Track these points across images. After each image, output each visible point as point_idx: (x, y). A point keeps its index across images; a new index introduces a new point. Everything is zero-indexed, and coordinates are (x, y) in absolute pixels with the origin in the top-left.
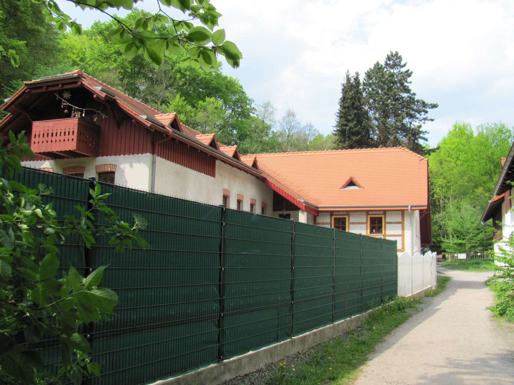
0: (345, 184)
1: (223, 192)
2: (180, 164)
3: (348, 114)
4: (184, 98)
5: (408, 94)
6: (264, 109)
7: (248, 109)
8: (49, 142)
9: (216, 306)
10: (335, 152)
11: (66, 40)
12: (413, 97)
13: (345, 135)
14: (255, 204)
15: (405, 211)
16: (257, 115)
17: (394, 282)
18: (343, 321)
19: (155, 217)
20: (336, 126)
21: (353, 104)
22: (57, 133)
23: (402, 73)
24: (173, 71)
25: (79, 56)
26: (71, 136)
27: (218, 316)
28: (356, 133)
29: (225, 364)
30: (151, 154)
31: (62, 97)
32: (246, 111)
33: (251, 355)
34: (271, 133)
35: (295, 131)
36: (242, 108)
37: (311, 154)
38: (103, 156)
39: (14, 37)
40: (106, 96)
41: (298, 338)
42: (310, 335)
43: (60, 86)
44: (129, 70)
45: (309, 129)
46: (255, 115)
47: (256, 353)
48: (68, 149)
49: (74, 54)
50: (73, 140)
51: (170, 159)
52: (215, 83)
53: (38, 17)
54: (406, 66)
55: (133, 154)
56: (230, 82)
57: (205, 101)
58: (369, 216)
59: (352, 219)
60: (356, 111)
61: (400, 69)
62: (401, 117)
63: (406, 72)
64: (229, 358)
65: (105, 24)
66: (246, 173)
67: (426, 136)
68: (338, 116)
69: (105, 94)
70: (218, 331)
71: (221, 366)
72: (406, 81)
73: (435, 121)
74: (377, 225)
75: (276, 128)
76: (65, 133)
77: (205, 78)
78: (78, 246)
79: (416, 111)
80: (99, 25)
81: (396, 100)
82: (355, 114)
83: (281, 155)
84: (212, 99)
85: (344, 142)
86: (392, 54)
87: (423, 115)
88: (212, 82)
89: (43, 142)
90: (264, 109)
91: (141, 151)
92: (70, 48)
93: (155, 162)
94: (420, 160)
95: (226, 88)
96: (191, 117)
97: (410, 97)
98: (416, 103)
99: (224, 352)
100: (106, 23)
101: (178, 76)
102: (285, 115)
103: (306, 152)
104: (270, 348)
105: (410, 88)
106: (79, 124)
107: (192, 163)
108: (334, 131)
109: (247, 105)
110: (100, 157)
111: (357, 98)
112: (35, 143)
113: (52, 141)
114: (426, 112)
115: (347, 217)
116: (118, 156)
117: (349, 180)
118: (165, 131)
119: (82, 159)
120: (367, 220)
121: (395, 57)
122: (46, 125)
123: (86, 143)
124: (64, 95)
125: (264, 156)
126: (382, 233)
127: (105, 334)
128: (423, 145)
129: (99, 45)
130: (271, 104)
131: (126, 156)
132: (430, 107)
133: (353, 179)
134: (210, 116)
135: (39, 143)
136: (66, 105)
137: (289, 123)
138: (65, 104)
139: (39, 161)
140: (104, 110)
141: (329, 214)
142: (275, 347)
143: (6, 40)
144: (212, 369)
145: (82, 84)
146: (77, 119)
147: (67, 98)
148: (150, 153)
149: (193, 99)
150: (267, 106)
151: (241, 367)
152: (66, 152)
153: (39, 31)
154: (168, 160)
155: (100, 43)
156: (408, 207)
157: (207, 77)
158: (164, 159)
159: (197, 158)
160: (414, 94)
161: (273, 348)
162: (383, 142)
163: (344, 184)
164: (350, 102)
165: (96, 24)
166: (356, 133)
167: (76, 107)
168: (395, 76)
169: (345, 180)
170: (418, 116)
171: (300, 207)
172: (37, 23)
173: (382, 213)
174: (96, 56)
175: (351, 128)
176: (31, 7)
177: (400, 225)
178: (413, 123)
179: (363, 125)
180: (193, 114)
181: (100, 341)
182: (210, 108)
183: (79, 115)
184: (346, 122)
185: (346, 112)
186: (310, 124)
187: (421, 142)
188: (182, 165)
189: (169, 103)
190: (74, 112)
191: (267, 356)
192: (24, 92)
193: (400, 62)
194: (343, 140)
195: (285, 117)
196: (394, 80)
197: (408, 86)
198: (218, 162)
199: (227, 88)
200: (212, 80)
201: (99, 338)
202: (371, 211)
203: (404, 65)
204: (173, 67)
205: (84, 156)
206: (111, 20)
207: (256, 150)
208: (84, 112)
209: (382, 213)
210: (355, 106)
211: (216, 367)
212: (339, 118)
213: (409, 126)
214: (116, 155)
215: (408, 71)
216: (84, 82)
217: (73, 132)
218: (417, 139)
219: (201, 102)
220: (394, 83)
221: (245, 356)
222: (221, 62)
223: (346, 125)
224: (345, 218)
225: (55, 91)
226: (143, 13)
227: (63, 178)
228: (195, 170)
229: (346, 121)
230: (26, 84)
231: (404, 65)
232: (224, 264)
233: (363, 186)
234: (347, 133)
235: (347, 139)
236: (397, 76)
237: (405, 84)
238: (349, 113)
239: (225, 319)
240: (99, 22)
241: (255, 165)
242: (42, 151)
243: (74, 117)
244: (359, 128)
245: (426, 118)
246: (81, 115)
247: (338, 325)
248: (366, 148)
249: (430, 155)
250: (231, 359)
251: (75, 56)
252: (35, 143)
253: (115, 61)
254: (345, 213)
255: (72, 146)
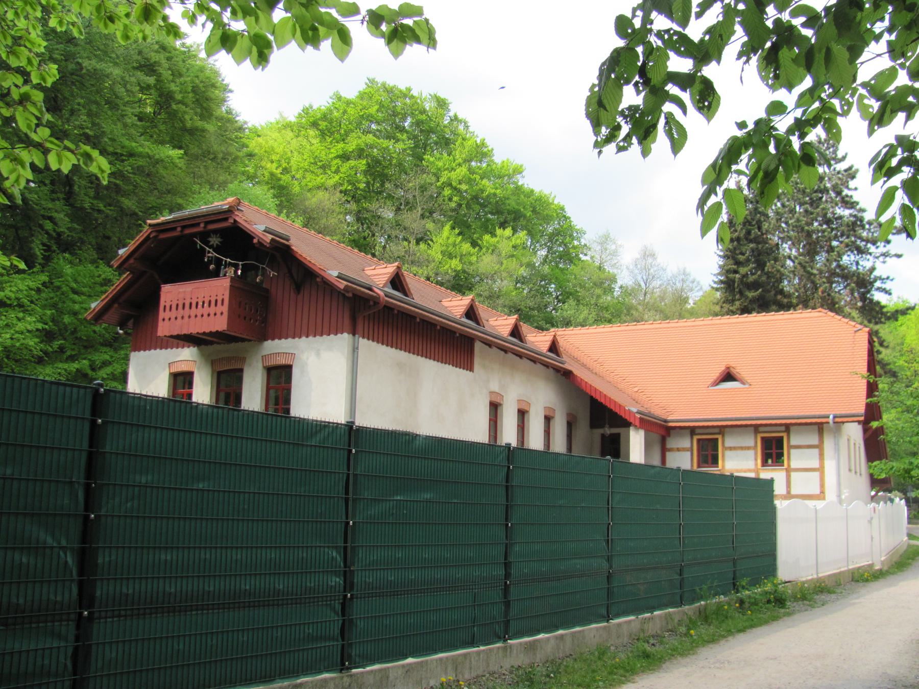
0: (718, 378)
1: (490, 396)
2: (405, 351)
3: (738, 252)
4: (457, 231)
5: (851, 211)
6: (599, 247)
7: (574, 248)
8: (205, 316)
9: (337, 581)
10: (717, 320)
11: (260, 140)
12: (859, 215)
13: (734, 289)
14: (553, 417)
15: (825, 425)
16: (592, 258)
17: (772, 555)
18: (632, 618)
19: (192, 439)
20: (719, 274)
21: (749, 232)
22: (197, 303)
23: (839, 173)
24: (439, 184)
25: (280, 166)
26: (220, 308)
27: (341, 597)
28: (755, 286)
29: (351, 676)
30: (351, 335)
31: (207, 243)
32: (571, 251)
33: (410, 664)
34: (617, 289)
35: (656, 283)
36: (565, 245)
37: (661, 326)
38: (273, 339)
39: (162, 143)
40: (272, 240)
41: (521, 644)
42: (548, 639)
43: (202, 225)
44: (362, 186)
45: (683, 280)
46: (587, 258)
47: (422, 662)
48: (214, 330)
49: (272, 162)
50: (222, 313)
51: (385, 341)
52: (512, 203)
53: (203, 108)
54: (847, 159)
55: (322, 335)
56: (540, 200)
57: (496, 236)
58: (695, 438)
59: (730, 441)
60: (752, 245)
61: (835, 166)
62: (835, 253)
63: (846, 171)
64: (363, 666)
65: (320, 110)
66: (532, 363)
67: (888, 285)
68: (720, 256)
69: (270, 237)
70: (341, 622)
71: (343, 677)
72: (847, 187)
73: (903, 257)
74: (774, 451)
75: (624, 279)
76: (210, 302)
77: (495, 195)
78: (71, 483)
79: (867, 241)
80: (310, 111)
81: (828, 222)
82: (753, 250)
83: (632, 327)
84: (508, 232)
85: (732, 302)
86: (820, 139)
87: (882, 248)
88: (507, 202)
89: (176, 318)
90: (599, 247)
91: (333, 329)
92: (265, 152)
93: (357, 348)
94: (856, 332)
95: (532, 211)
96: (471, 264)
97: (855, 216)
98: (867, 226)
99: (353, 657)
100: (323, 108)
101: (447, 192)
102: (638, 256)
103: (676, 320)
104: (454, 656)
105: (855, 199)
106: (232, 287)
107: (420, 348)
108: (715, 282)
109: (572, 240)
110: (270, 341)
111: (754, 223)
112: (164, 320)
113: (190, 317)
114: (888, 242)
115: (720, 437)
116: (297, 339)
117: (724, 371)
118: (372, 296)
119: (240, 345)
120: (756, 442)
121: (826, 145)
122: (181, 290)
123: (245, 318)
124: (210, 239)
125: (578, 332)
126: (783, 466)
127: (116, 613)
128: (883, 303)
129: (312, 145)
130: (612, 236)
131: (311, 338)
132: (894, 231)
133: (731, 369)
134: (505, 262)
135: (170, 319)
136: (212, 257)
137: (646, 269)
138: (210, 255)
139: (174, 349)
140: (273, 264)
141: (688, 431)
142: (465, 655)
143: (150, 149)
144: (325, 681)
145: (235, 221)
146: (229, 280)
147: (215, 246)
148: (349, 333)
149: (474, 233)
150: (605, 240)
151: (387, 683)
152: (211, 334)
153: (204, 130)
154: (383, 344)
155: (314, 141)
156: (828, 417)
157: (498, 191)
158: (375, 343)
159: (437, 338)
160: (863, 211)
161: (459, 655)
162: (805, 303)
163: (715, 377)
164: (742, 229)
165: (306, 111)
166: (755, 286)
167: (228, 260)
168: (826, 179)
169: (718, 371)
170: (872, 249)
171: (631, 421)
172: (202, 117)
173: (783, 428)
174: (306, 164)
175: (745, 276)
176: (193, 91)
177: (816, 451)
178: (861, 263)
179: (766, 269)
180: (474, 259)
181: (106, 622)
182: (505, 247)
183: (233, 272)
184: (735, 267)
185: (735, 249)
186: (684, 270)
187: (878, 296)
188: (409, 352)
189: (432, 241)
190: (225, 268)
191: (446, 668)
192: (148, 237)
193: (835, 152)
194: (731, 298)
195: (637, 259)
196: (822, 187)
197: (851, 197)
198: (478, 346)
199: (534, 211)
200: (508, 199)
201: (106, 618)
202: (761, 425)
203: (844, 158)
204: (438, 178)
205: (243, 340)
206: (331, 103)
207: (585, 320)
208: (240, 267)
209: (783, 428)
210: (752, 236)
211: (332, 679)
212: (722, 259)
213: (854, 268)
214: (294, 338)
215: (850, 168)
216: (238, 219)
217: (223, 300)
218: (869, 292)
219: (487, 237)
220: (826, 191)
221: (398, 667)
222: (521, 166)
223: (736, 272)
224: (717, 439)
225: (195, 235)
226: (385, 87)
227: (47, 385)
228: (434, 360)
229: (735, 265)
230: (150, 225)
231: (844, 158)
232: (354, 516)
233: (749, 381)
234: (736, 285)
235: (737, 297)
236: (829, 179)
237: (845, 192)
238: (739, 249)
239: (355, 603)
240: (311, 107)
241: (554, 348)
242: (175, 333)
243: (225, 275)
244: (759, 276)
245: (887, 252)
246: (236, 272)
247: (619, 625)
248: (758, 313)
249: (897, 320)
250: (368, 668)
251: (275, 165)
252: (164, 320)
253: (337, 171)
254: (717, 430)
255: (220, 324)
